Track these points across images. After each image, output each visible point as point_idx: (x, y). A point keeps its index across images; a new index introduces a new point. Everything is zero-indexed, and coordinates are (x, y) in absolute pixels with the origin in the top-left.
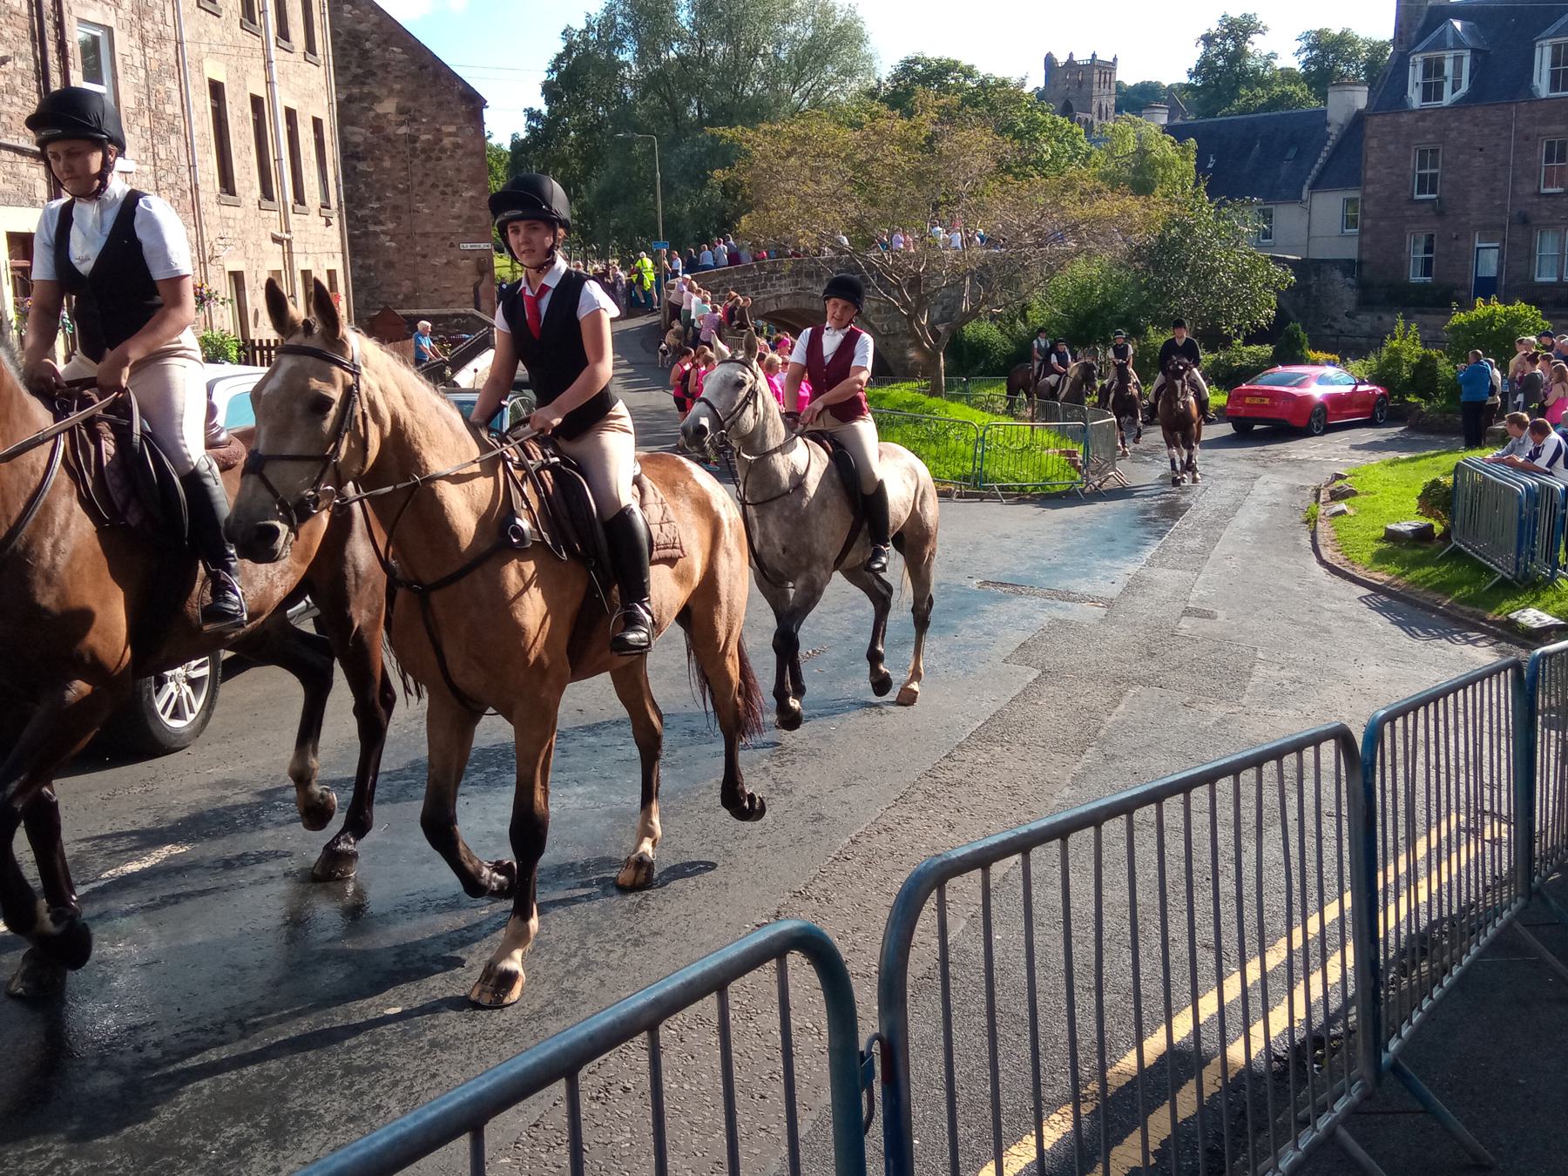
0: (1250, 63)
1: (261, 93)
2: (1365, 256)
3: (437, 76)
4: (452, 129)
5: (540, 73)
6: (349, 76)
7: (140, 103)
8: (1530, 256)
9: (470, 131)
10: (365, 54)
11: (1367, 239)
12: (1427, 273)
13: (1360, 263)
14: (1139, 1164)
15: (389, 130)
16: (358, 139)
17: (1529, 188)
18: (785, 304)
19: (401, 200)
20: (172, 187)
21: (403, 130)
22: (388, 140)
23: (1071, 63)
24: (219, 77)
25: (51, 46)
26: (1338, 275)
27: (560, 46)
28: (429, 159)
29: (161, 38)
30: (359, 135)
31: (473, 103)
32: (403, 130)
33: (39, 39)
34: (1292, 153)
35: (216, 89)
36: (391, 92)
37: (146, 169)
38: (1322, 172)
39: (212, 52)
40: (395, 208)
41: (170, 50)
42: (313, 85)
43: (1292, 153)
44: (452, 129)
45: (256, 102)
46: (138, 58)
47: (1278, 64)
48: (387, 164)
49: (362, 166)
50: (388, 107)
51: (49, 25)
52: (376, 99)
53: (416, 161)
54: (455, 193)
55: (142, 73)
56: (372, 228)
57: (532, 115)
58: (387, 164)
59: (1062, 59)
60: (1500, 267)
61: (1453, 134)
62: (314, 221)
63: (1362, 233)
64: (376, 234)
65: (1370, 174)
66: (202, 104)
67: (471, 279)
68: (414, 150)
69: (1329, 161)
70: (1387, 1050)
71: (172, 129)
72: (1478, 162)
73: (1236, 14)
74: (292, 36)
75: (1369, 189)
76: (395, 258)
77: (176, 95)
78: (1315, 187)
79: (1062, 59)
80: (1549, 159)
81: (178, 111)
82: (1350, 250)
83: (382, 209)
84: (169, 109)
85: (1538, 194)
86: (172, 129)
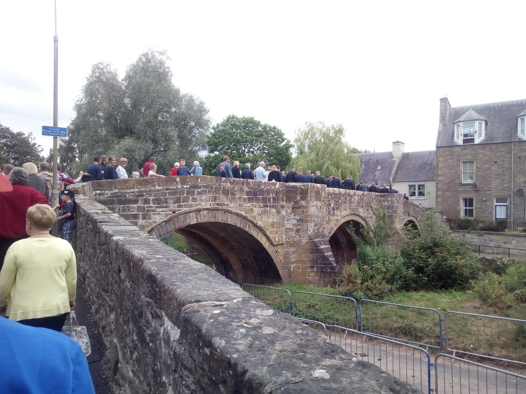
18: (205, 218)
34: (379, 168)
43: (379, 168)
72: (494, 168)
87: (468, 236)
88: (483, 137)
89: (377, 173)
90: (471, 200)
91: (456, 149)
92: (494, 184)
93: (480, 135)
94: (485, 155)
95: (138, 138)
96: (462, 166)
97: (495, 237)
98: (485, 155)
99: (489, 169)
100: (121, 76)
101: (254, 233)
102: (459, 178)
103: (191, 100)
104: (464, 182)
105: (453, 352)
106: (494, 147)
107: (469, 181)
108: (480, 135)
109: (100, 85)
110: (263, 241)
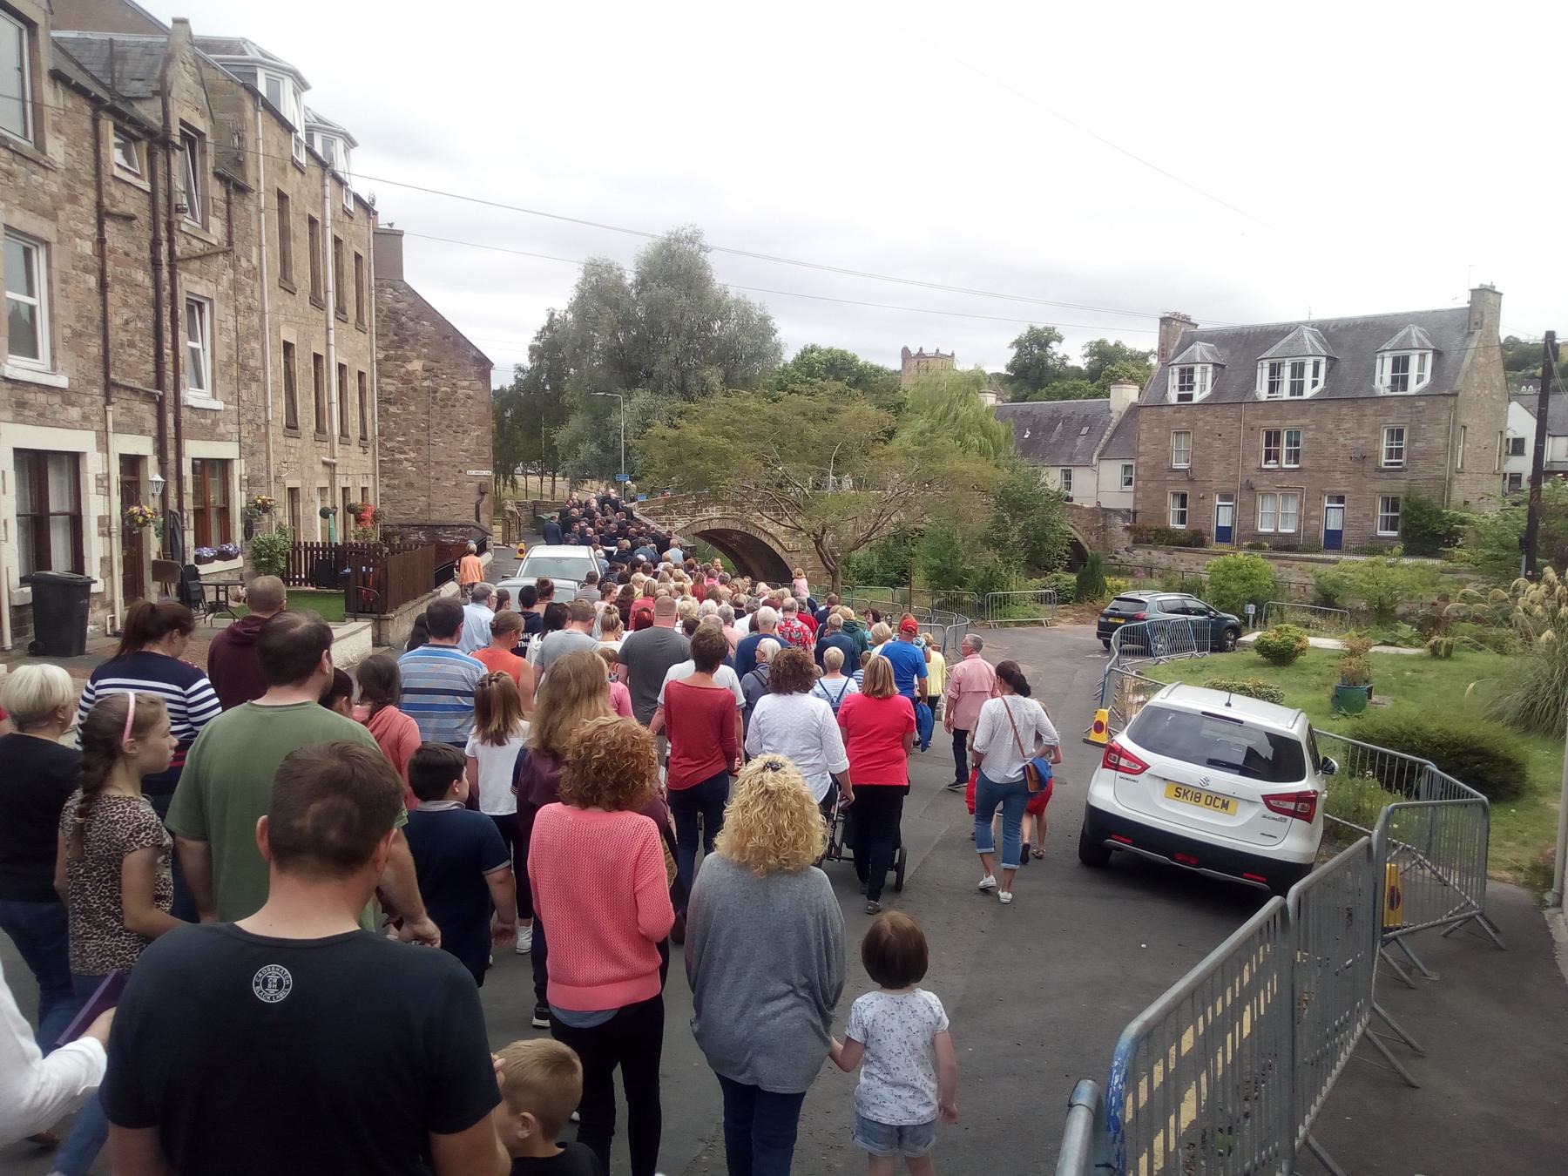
0: (1050, 362)
1: (322, 352)
2: (1139, 507)
3: (456, 344)
4: (466, 383)
5: (528, 338)
6: (387, 341)
7: (230, 357)
8: (1255, 513)
9: (479, 385)
10: (401, 325)
11: (1139, 495)
12: (1182, 521)
13: (1135, 513)
14: (342, 603)
15: (416, 384)
16: (391, 388)
17: (1255, 464)
18: (716, 525)
19: (423, 437)
20: (250, 422)
21: (426, 383)
22: (414, 390)
23: (920, 355)
24: (292, 340)
25: (166, 311)
26: (1119, 520)
27: (544, 321)
28: (445, 406)
29: (249, 308)
30: (391, 386)
31: (484, 366)
32: (426, 383)
33: (157, 305)
34: (1085, 430)
35: (288, 347)
36: (418, 357)
37: (231, 407)
38: (1107, 445)
39: (287, 321)
40: (417, 441)
41: (255, 319)
42: (360, 347)
43: (1085, 430)
44: (466, 383)
45: (317, 358)
46: (231, 324)
47: (1069, 363)
48: (413, 408)
49: (392, 409)
50: (416, 365)
51: (165, 294)
52: (407, 360)
53: (437, 408)
54: (465, 432)
55: (233, 335)
56: (398, 456)
57: (520, 369)
58: (413, 408)
59: (914, 351)
60: (1234, 521)
61: (1200, 423)
62: (354, 449)
63: (1137, 490)
64: (400, 462)
65: (1141, 448)
66: (275, 360)
67: (474, 498)
68: (434, 398)
69: (1110, 439)
70: (117, 146)
71: (255, 379)
72: (1218, 444)
73: (1040, 327)
74: (348, 311)
75: (1141, 459)
76: (414, 479)
77: (258, 352)
78: (1101, 457)
79: (914, 351)
80: (1268, 444)
81: (259, 364)
82: (1126, 502)
83: (406, 443)
84: (252, 363)
85: (1262, 469)
86: (255, 379)
87: (1154, 553)
88: (1209, 390)
89: (1080, 441)
90: (1184, 497)
91: (1166, 410)
92: (1217, 469)
93: (1203, 388)
94: (1206, 423)
95: (657, 390)
96: (1173, 438)
97: (1186, 556)
98: (1206, 423)
99: (1210, 446)
100: (630, 278)
101: (765, 539)
102: (1168, 459)
103: (746, 312)
104: (1176, 466)
105: (1136, 738)
106: (1218, 409)
107: (1184, 466)
108: (1203, 388)
109: (599, 292)
110: (775, 547)
